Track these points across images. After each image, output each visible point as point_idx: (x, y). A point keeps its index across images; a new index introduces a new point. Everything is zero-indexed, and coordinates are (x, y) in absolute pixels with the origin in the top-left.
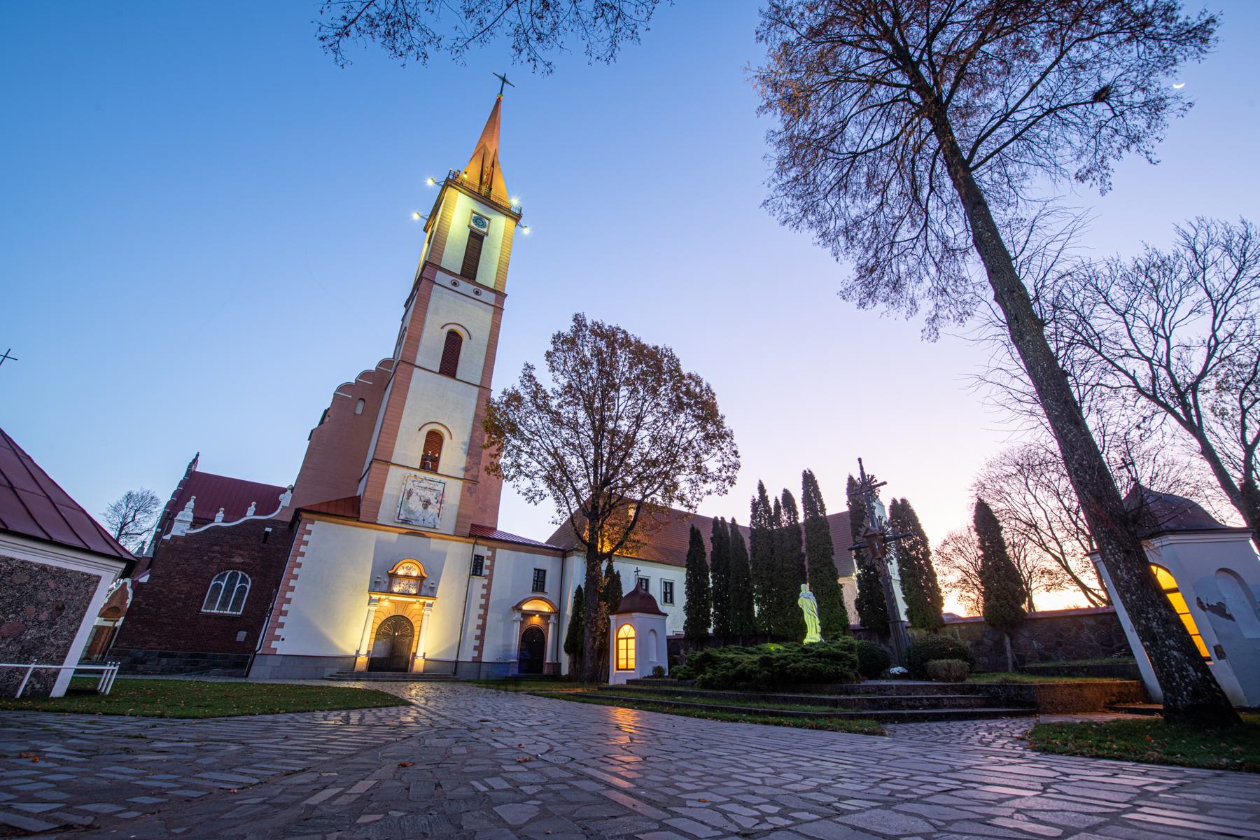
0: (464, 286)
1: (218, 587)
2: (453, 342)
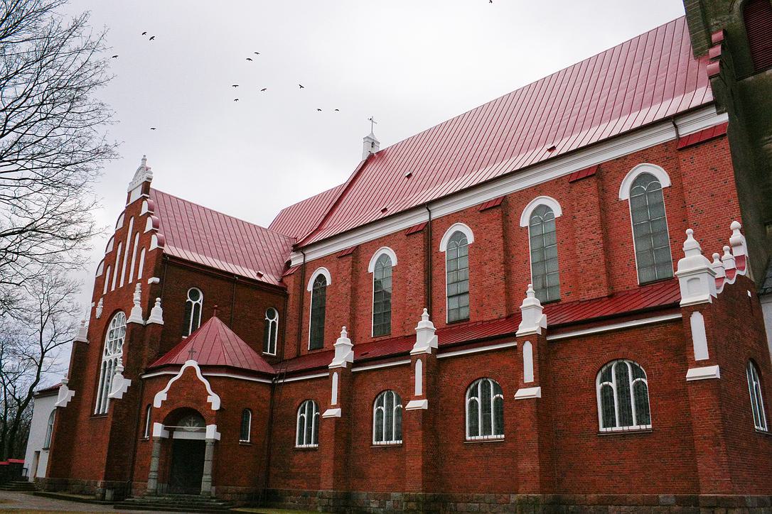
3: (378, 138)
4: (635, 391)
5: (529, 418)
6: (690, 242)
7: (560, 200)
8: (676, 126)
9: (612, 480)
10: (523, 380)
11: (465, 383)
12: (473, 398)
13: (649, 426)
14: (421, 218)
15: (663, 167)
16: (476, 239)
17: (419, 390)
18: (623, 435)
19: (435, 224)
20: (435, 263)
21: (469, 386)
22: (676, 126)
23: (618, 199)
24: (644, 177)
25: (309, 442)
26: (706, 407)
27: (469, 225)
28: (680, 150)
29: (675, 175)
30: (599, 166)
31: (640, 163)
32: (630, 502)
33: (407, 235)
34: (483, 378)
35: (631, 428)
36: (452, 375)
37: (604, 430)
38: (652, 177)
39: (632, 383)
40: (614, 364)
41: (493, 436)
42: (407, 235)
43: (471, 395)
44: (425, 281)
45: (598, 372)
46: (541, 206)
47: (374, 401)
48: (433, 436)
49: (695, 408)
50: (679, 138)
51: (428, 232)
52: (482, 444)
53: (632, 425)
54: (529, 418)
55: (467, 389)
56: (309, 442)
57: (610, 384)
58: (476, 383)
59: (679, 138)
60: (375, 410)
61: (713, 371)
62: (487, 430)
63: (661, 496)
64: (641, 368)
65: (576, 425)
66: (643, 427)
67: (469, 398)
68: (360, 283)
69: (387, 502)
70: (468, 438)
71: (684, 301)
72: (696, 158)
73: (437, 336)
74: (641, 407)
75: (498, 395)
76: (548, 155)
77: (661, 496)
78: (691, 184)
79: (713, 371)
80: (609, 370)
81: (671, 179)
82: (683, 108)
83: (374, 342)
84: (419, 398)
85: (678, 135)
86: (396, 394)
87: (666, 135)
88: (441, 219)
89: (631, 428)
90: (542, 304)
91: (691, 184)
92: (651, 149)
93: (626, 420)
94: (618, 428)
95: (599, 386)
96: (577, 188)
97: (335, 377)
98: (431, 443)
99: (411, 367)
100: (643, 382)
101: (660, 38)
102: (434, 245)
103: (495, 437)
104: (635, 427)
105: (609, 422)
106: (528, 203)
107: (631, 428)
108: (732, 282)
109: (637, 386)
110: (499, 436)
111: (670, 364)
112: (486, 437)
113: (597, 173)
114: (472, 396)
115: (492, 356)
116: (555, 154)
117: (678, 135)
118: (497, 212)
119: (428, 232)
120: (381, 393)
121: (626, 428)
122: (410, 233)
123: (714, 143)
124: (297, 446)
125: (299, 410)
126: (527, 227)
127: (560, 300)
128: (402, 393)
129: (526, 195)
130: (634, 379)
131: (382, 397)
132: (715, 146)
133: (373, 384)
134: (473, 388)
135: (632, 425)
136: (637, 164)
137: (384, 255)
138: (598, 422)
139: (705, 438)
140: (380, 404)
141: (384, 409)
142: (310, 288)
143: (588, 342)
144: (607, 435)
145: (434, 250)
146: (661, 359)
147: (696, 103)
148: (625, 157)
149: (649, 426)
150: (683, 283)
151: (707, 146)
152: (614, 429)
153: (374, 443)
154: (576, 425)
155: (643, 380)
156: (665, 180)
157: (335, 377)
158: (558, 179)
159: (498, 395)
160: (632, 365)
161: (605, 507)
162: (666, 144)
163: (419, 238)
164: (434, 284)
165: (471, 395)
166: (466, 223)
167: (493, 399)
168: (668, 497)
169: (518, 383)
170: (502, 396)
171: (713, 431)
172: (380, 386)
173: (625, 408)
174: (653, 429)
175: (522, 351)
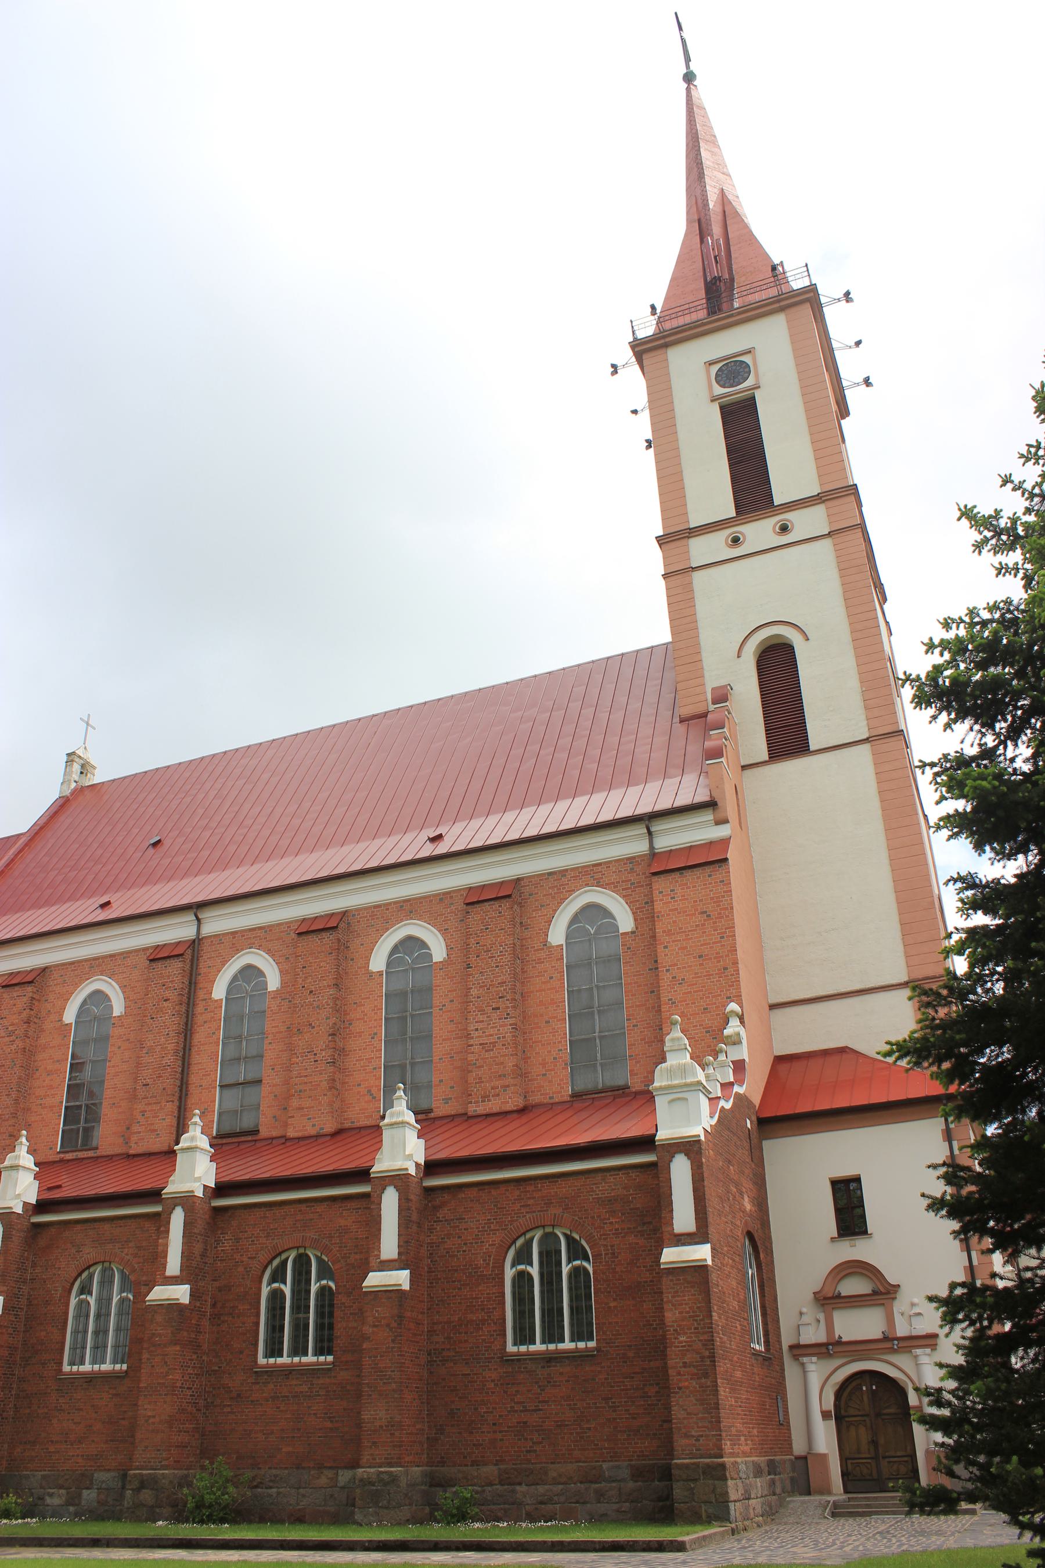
0: (759, 532)
1: (276, 1297)
2: (777, 663)
3: (92, 758)
4: (317, 1300)
5: (388, 1325)
6: (675, 1037)
7: (444, 932)
8: (650, 833)
9: (526, 1439)
10: (379, 1256)
11: (263, 1256)
12: (276, 1285)
13: (592, 1344)
14: (178, 931)
15: (624, 897)
16: (284, 983)
17: (173, 1264)
18: (549, 1359)
19: (206, 947)
20: (199, 1019)
21: (270, 1262)
22: (650, 833)
23: (545, 942)
24: (411, 943)
25: (298, 1349)
26: (688, 1312)
27: (272, 956)
28: (654, 874)
29: (646, 914)
30: (518, 880)
31: (587, 885)
32: (554, 1478)
33: (151, 960)
34: (298, 1248)
35: (561, 1346)
36: (238, 1240)
37: (514, 1349)
38: (606, 913)
39: (565, 1269)
40: (538, 1235)
41: (310, 1359)
42: (151, 960)
43: (273, 1279)
44: (176, 1052)
45: (510, 1247)
46: (410, 938)
47: (73, 1284)
48: (194, 1357)
49: (671, 1316)
50: (653, 855)
51: (191, 958)
52: (291, 1372)
53: (534, 1343)
54: (388, 1325)
55: (266, 1267)
56: (298, 1349)
57: (529, 1268)
58: (284, 1256)
59: (653, 855)
60: (73, 1301)
61: (402, 1278)
62: (553, 1334)
63: (605, 1466)
64: (583, 1243)
65: (466, 1341)
66: (581, 1345)
67: (269, 1284)
68: (42, 1041)
69: (85, 1492)
70: (262, 1360)
71: (661, 1135)
72: (679, 891)
73: (422, 1142)
74: (325, 1327)
75: (324, 1282)
76: (428, 850)
77: (605, 1466)
78: (669, 933)
79: (402, 1278)
80: (529, 1244)
81: (635, 920)
82: (664, 804)
83: (61, 1161)
84: (386, 1266)
85: (651, 846)
86: (122, 1273)
87: (631, 845)
88: (218, 937)
89: (561, 1346)
90: (36, 1164)
91: (669, 933)
92: (608, 864)
93: (553, 1334)
94: (538, 1347)
95: (509, 1273)
96: (477, 914)
97: (177, 1219)
98: (190, 1370)
99: (161, 1221)
100: (585, 1270)
101: (627, 671)
102: (201, 986)
103: (315, 1359)
104: (568, 1345)
105: (524, 1335)
106: (388, 929)
107: (561, 1346)
108: (728, 1105)
109: (577, 1273)
110: (322, 1358)
111: (632, 1239)
112: (96, 1367)
113: (504, 894)
114: (82, 1293)
115: (320, 1208)
116: (442, 848)
117: (651, 846)
118: (328, 938)
119: (191, 958)
120: (89, 1267)
121: (552, 1347)
122: (158, 956)
123: (708, 870)
124: (511, 1348)
125: (511, 1254)
126: (380, 973)
127: (430, 1111)
128: (133, 1271)
129: (562, 882)
130: (569, 1261)
131: (91, 1277)
132: (710, 876)
133: (73, 1250)
134: (277, 1267)
135: (534, 1343)
136: (582, 887)
137: (98, 992)
138: (505, 1335)
139: (685, 1365)
140: (86, 1289)
141: (92, 1300)
142: (219, 991)
143: (494, 1192)
144: (518, 1360)
145: (201, 994)
146: (617, 1230)
147: (683, 800)
148: (563, 872)
149: (592, 1344)
150: (660, 1102)
151: (698, 872)
152: (532, 1348)
153: (66, 1368)
154: (466, 1341)
155: (585, 1264)
156: (625, 921)
157: (177, 1219)
158: (444, 894)
159: (324, 1282)
160: (568, 1237)
161: (511, 1488)
162: (631, 860)
163: (174, 970)
164: (196, 1058)
165: (273, 1279)
166: (269, 952)
167: (314, 1288)
168: (618, 1467)
169: (156, 1275)
170: (332, 1284)
171: (698, 1353)
172: (89, 1253)
173: (552, 1314)
174: (598, 1349)
175: (380, 1204)
